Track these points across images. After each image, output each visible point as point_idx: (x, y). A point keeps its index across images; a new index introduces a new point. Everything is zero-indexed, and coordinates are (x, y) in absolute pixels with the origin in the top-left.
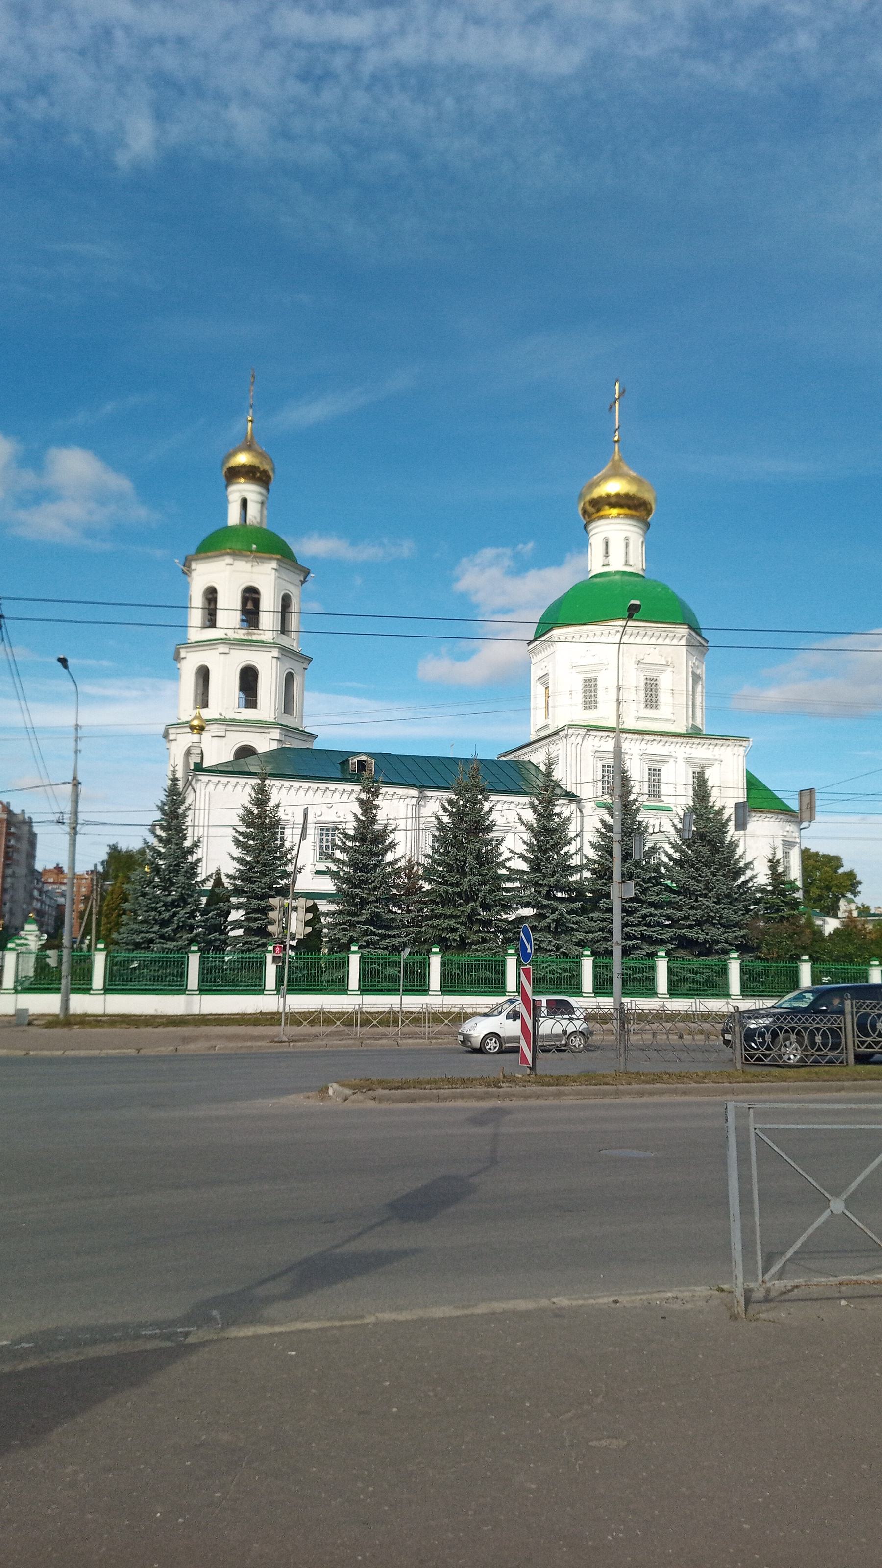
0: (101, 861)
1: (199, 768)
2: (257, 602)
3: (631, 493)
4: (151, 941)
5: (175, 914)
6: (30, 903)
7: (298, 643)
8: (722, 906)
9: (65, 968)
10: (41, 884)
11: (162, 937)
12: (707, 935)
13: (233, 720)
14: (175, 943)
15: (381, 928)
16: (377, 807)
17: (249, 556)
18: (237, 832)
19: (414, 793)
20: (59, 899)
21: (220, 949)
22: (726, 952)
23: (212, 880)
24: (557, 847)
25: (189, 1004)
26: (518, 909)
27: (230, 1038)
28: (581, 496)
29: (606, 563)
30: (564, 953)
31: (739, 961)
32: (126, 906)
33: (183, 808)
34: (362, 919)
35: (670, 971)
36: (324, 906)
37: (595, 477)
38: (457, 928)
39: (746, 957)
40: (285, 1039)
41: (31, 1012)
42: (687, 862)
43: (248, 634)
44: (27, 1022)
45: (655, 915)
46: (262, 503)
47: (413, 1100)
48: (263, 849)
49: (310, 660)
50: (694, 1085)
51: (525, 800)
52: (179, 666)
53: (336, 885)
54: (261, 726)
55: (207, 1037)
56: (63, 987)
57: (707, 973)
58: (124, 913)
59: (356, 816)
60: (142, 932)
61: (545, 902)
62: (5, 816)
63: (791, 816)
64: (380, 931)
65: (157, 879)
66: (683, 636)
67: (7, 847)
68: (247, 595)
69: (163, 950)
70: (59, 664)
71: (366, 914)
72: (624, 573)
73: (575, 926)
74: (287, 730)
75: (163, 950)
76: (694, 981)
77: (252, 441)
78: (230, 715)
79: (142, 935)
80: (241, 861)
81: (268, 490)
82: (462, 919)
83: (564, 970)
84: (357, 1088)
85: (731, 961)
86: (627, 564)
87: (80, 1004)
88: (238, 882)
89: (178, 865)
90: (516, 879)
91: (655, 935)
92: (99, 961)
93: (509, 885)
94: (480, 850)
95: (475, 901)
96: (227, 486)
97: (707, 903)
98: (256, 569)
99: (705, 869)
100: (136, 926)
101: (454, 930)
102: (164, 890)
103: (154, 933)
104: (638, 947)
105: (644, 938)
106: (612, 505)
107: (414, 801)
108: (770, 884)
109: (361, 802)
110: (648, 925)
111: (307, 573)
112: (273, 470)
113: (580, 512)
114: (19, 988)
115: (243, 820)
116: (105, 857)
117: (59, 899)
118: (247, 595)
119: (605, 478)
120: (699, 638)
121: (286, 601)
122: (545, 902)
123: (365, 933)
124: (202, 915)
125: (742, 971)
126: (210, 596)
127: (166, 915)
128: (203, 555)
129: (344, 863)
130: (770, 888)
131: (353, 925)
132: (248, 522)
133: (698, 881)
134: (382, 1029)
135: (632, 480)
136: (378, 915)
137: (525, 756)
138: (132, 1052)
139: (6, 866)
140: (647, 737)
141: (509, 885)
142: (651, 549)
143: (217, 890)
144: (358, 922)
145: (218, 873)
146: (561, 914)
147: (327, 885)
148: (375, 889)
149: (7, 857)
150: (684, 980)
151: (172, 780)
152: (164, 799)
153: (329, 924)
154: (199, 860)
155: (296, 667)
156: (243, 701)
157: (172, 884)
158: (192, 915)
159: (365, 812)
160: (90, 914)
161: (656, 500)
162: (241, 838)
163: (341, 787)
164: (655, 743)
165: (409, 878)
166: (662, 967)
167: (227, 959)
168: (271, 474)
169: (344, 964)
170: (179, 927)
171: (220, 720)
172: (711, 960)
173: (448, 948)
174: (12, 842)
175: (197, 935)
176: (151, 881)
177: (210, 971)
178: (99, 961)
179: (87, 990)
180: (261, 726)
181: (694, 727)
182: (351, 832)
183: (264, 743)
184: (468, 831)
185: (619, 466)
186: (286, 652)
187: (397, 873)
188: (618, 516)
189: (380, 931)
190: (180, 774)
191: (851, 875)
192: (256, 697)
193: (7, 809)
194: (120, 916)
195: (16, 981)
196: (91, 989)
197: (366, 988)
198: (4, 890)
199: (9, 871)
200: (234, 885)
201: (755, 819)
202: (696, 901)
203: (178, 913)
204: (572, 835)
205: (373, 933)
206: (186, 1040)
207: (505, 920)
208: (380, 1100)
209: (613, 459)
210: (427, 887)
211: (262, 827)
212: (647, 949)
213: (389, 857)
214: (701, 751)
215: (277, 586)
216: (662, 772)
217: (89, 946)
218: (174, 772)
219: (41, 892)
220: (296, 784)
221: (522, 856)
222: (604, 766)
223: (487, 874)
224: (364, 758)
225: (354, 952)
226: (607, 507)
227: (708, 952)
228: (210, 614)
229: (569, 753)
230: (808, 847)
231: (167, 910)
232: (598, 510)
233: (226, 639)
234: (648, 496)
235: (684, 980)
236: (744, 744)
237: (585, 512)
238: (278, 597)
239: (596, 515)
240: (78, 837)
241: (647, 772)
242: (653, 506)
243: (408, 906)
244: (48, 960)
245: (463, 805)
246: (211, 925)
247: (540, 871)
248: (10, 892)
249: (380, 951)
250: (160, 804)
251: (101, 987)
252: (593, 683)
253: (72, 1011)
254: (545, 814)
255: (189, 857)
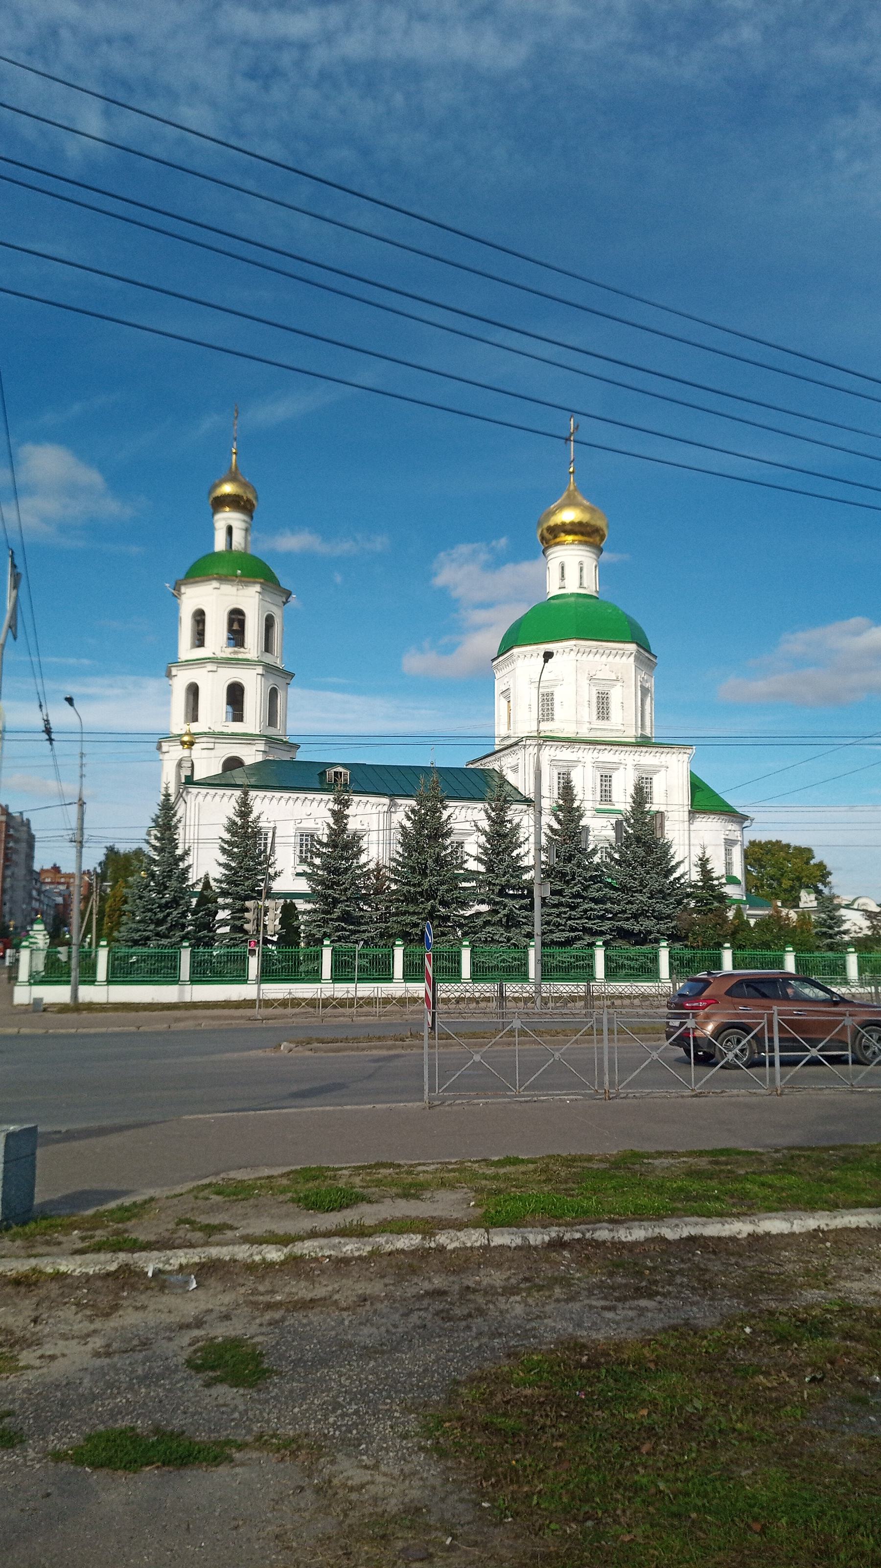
0: (99, 861)
1: (190, 781)
2: (242, 623)
3: (584, 521)
4: (148, 938)
5: (168, 915)
6: (29, 903)
7: (282, 659)
8: (654, 900)
9: (74, 962)
10: (39, 884)
11: (158, 934)
12: (642, 925)
13: (222, 734)
14: (169, 940)
15: (352, 924)
16: (347, 817)
17: (233, 581)
18: (223, 840)
19: (386, 800)
20: (57, 898)
21: (209, 944)
22: (657, 941)
23: (201, 884)
24: (508, 849)
25: (181, 993)
26: (473, 906)
27: (213, 1018)
28: (540, 524)
29: (562, 585)
30: (514, 944)
31: (856, 954)
32: (126, 907)
33: (175, 820)
34: (334, 916)
35: (607, 958)
36: (302, 905)
37: (552, 506)
38: (419, 924)
39: (677, 945)
40: (259, 1017)
41: (45, 1001)
42: (624, 862)
43: (235, 653)
44: (42, 1008)
45: (595, 910)
46: (246, 530)
47: (339, 1050)
48: (246, 856)
49: (292, 675)
50: (549, 1037)
51: (480, 805)
52: (171, 682)
53: (310, 886)
54: (247, 738)
55: (195, 1018)
56: (72, 979)
57: (642, 960)
58: (124, 915)
59: (328, 825)
60: (140, 931)
61: (498, 899)
62: (3, 818)
63: (733, 816)
64: (350, 927)
65: (152, 884)
66: (632, 653)
67: (6, 848)
68: (233, 616)
69: (159, 946)
70: (67, 703)
71: (337, 912)
72: (579, 595)
73: (524, 920)
74: (271, 741)
75: (159, 946)
76: (631, 968)
77: (236, 473)
78: (218, 729)
79: (140, 933)
80: (226, 866)
81: (252, 518)
82: (423, 915)
83: (515, 959)
84: (299, 1043)
85: (661, 949)
86: (581, 586)
87: (88, 994)
88: (224, 885)
89: (170, 871)
90: (473, 879)
91: (595, 927)
92: (103, 957)
93: (464, 884)
94: (439, 854)
95: (435, 899)
96: (213, 515)
97: (641, 898)
98: (241, 592)
99: (639, 868)
100: (134, 926)
101: (416, 925)
102: (159, 894)
103: (150, 931)
104: (580, 938)
105: (585, 930)
106: (568, 532)
107: (386, 808)
108: (701, 881)
109: (334, 813)
110: (589, 918)
111: (288, 594)
112: (257, 498)
113: (539, 538)
114: (32, 981)
115: (228, 830)
116: (102, 858)
117: (57, 898)
118: (233, 616)
119: (561, 507)
120: (647, 655)
121: (269, 623)
122: (498, 899)
123: (337, 929)
124: (192, 915)
125: (671, 957)
126: (199, 618)
127: (160, 916)
128: (191, 580)
129: (318, 867)
130: (700, 884)
131: (326, 921)
132: (233, 548)
133: (635, 879)
134: (341, 1010)
135: (585, 509)
136: (348, 912)
137: (492, 764)
138: (133, 1029)
139: (6, 867)
140: (599, 747)
141: (464, 884)
142: (603, 571)
143: (205, 893)
144: (332, 920)
145: (206, 877)
146: (511, 910)
147: (303, 886)
148: (346, 890)
149: (7, 858)
150: (623, 966)
151: (164, 795)
152: (158, 812)
153: (307, 921)
154: (190, 866)
155: (280, 682)
156: (230, 716)
157: (166, 888)
158: (183, 915)
159: (336, 822)
160: (91, 913)
161: (608, 526)
162: (226, 846)
163: (318, 797)
164: (606, 752)
165: (377, 879)
166: (600, 955)
167: (215, 953)
168: (254, 502)
169: (318, 957)
170: (172, 925)
171: (209, 733)
172: (646, 948)
173: (411, 941)
174: (11, 844)
175: (188, 933)
176: (148, 885)
177: (200, 963)
178: (103, 957)
179: (93, 982)
180: (247, 738)
181: (643, 736)
182: (325, 839)
183: (251, 755)
184: (429, 837)
185: (575, 497)
186: (269, 669)
187: (367, 875)
188: (573, 543)
189: (350, 927)
190: (172, 790)
191: (821, 866)
192: (242, 710)
193: (5, 811)
194: (120, 916)
195: (30, 976)
196: (95, 981)
197: (336, 978)
198: (4, 891)
199: (9, 873)
200: (221, 888)
201: (699, 820)
202: (632, 896)
203: (171, 913)
204: (522, 839)
205: (344, 929)
206: (178, 1020)
207: (462, 916)
208: (315, 1050)
209: (568, 490)
210: (394, 887)
211: (246, 836)
212: (588, 939)
213: (363, 859)
214: (648, 758)
215: (261, 608)
216: (613, 779)
217: (90, 944)
218: (167, 788)
219: (40, 892)
220: (278, 795)
221: (478, 859)
222: (559, 774)
223: (445, 875)
224: (340, 769)
225: (327, 946)
226: (563, 534)
227: (643, 942)
228: (199, 634)
229: (527, 762)
230: (779, 839)
231: (161, 911)
232: (555, 537)
233: (213, 658)
234: (600, 523)
235: (623, 966)
236: (688, 751)
237: (543, 538)
238: (262, 616)
239: (552, 542)
240: (84, 849)
241: (599, 778)
242: (606, 533)
243: (377, 905)
244: (59, 955)
245: (424, 814)
246: (201, 923)
247: (493, 871)
248: (10, 892)
249: (350, 945)
250: (154, 817)
251: (105, 979)
252: (550, 697)
253: (80, 1000)
254: (498, 821)
255: (181, 864)
